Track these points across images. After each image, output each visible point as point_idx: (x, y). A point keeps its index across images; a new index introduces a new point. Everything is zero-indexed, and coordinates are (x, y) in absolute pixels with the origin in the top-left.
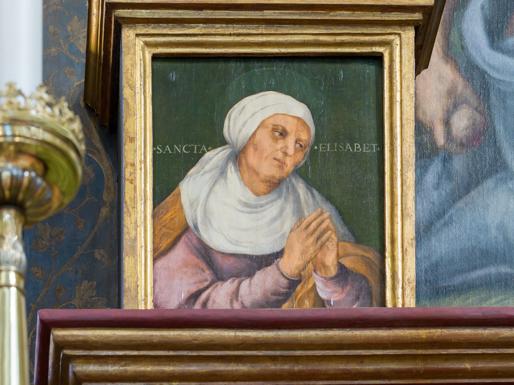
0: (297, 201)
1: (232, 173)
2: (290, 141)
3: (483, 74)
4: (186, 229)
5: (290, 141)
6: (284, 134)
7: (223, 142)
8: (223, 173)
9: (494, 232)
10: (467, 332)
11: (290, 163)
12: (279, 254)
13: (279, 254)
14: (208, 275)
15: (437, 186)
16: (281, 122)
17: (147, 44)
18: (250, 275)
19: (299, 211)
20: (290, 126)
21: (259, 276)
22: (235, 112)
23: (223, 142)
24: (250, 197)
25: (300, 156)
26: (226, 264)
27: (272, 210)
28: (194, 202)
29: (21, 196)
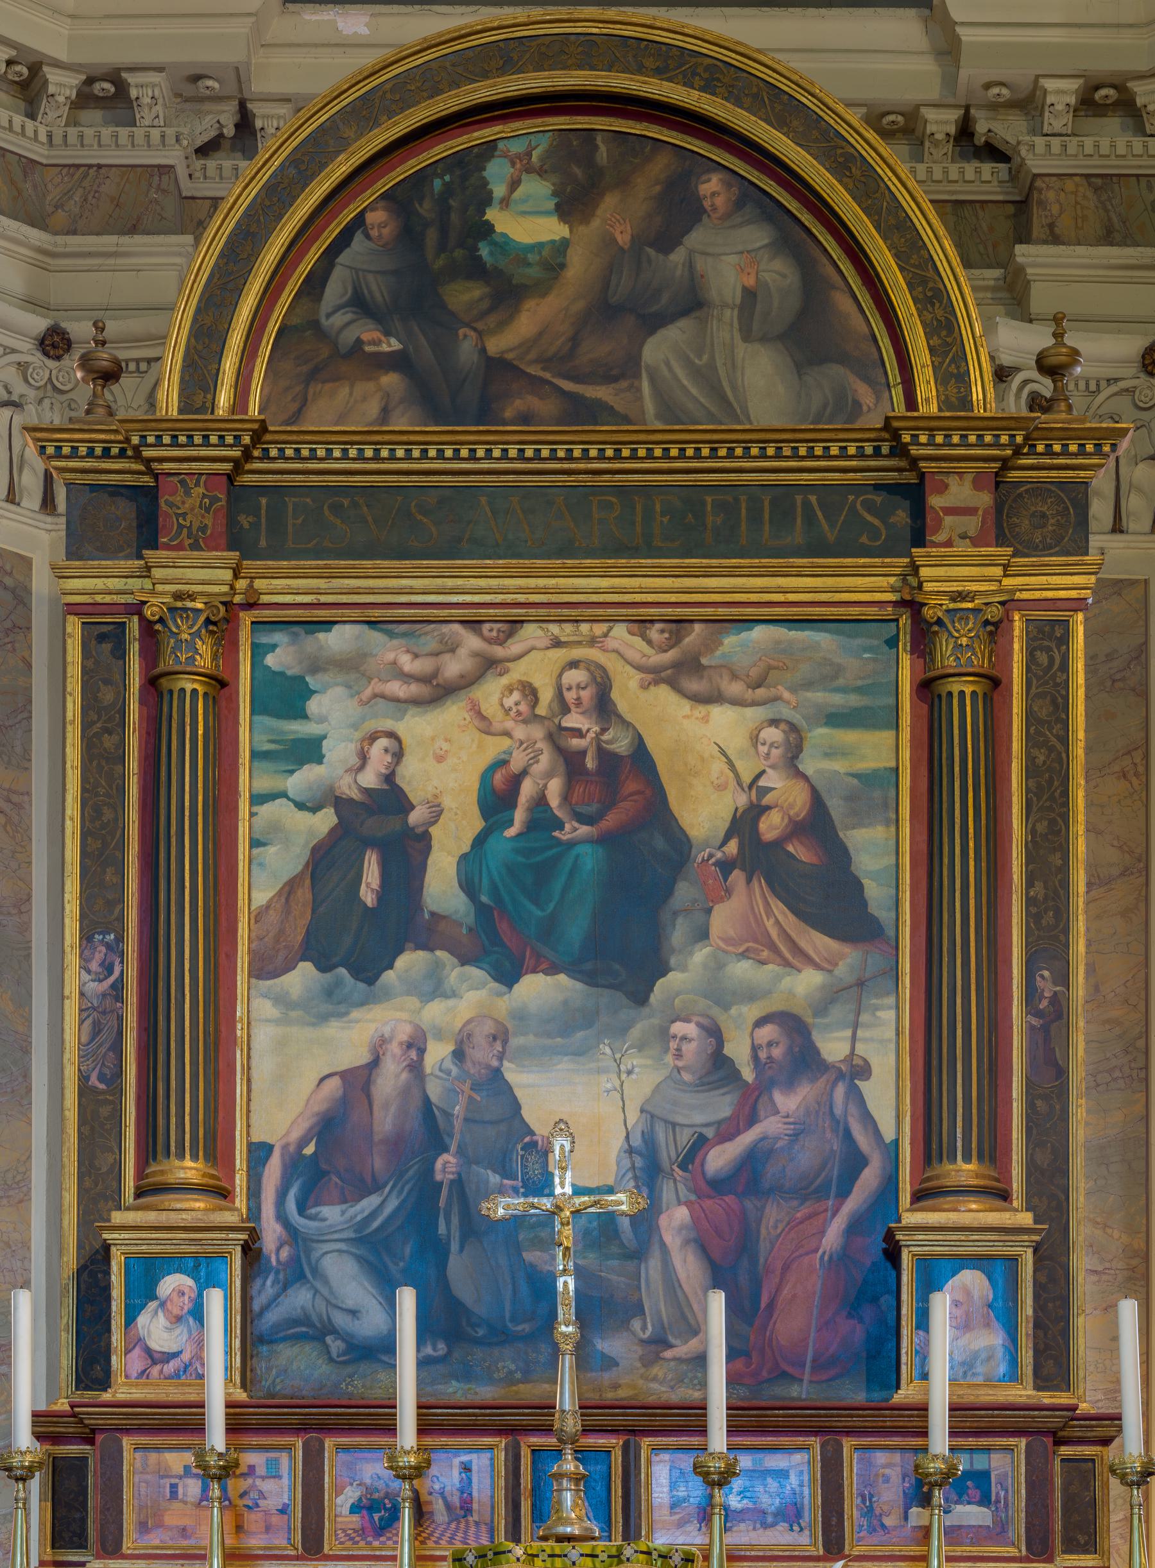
0: (189, 1325)
1: (160, 1314)
2: (186, 1298)
3: (295, 1228)
4: (140, 1340)
5: (186, 1298)
6: (183, 1294)
7: (157, 1298)
8: (156, 1313)
9: (299, 1311)
10: (251, 1410)
11: (186, 1308)
12: (181, 1352)
13: (181, 1352)
14: (149, 1362)
15: (272, 1286)
16: (182, 1288)
17: (155, 1159)
18: (168, 1362)
19: (190, 1332)
20: (187, 1291)
21: (172, 1363)
22: (161, 1283)
23: (157, 1298)
24: (168, 1324)
25: (191, 1305)
26: (156, 1356)
27: (178, 1331)
28: (427, 655)
29: (21, 1486)
